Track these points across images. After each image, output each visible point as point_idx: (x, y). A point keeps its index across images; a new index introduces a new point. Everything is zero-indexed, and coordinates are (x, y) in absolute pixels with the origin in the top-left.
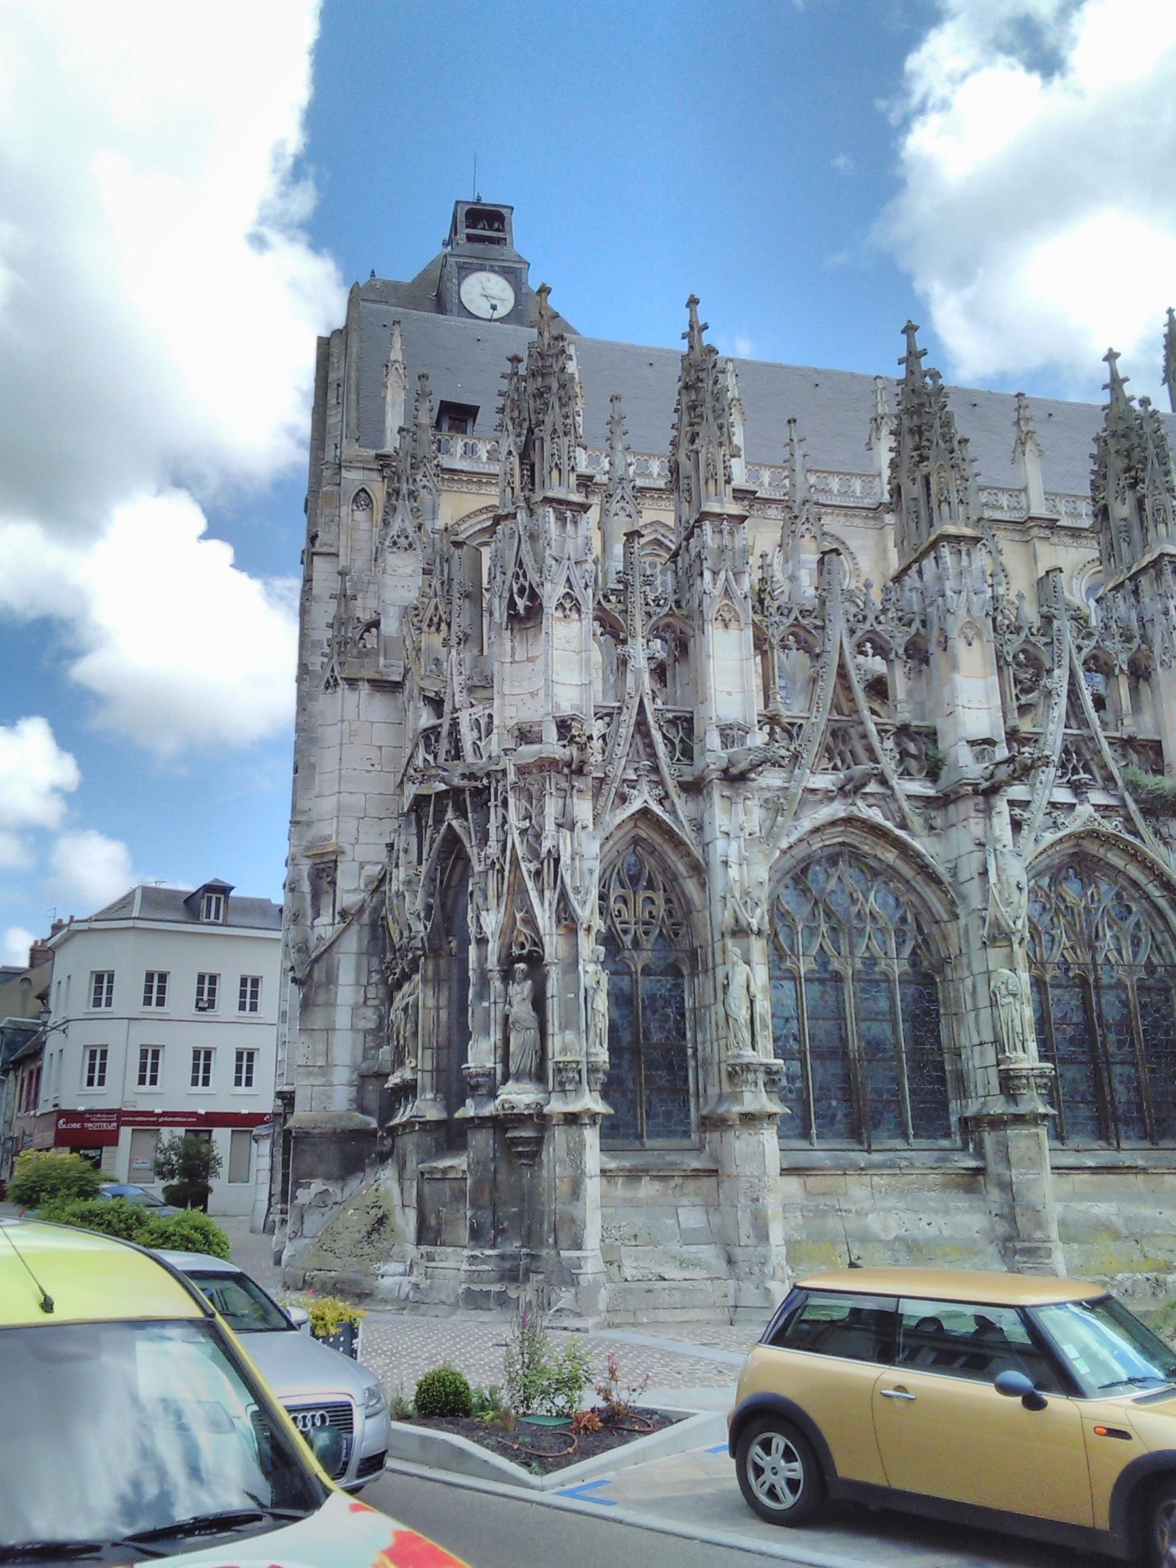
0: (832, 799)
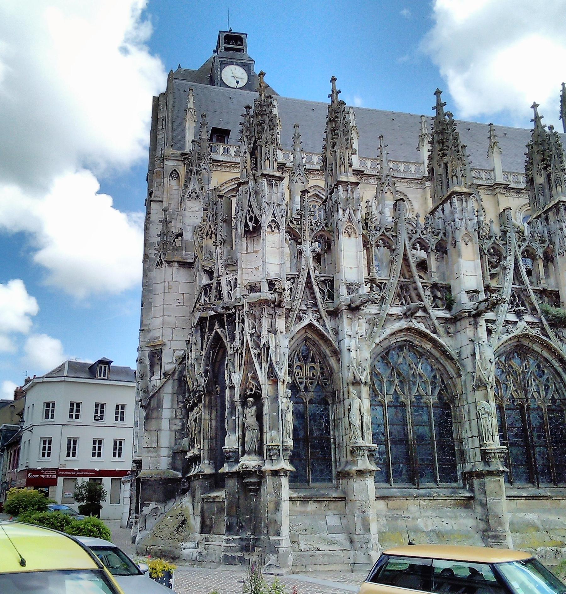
0: (400, 319)
